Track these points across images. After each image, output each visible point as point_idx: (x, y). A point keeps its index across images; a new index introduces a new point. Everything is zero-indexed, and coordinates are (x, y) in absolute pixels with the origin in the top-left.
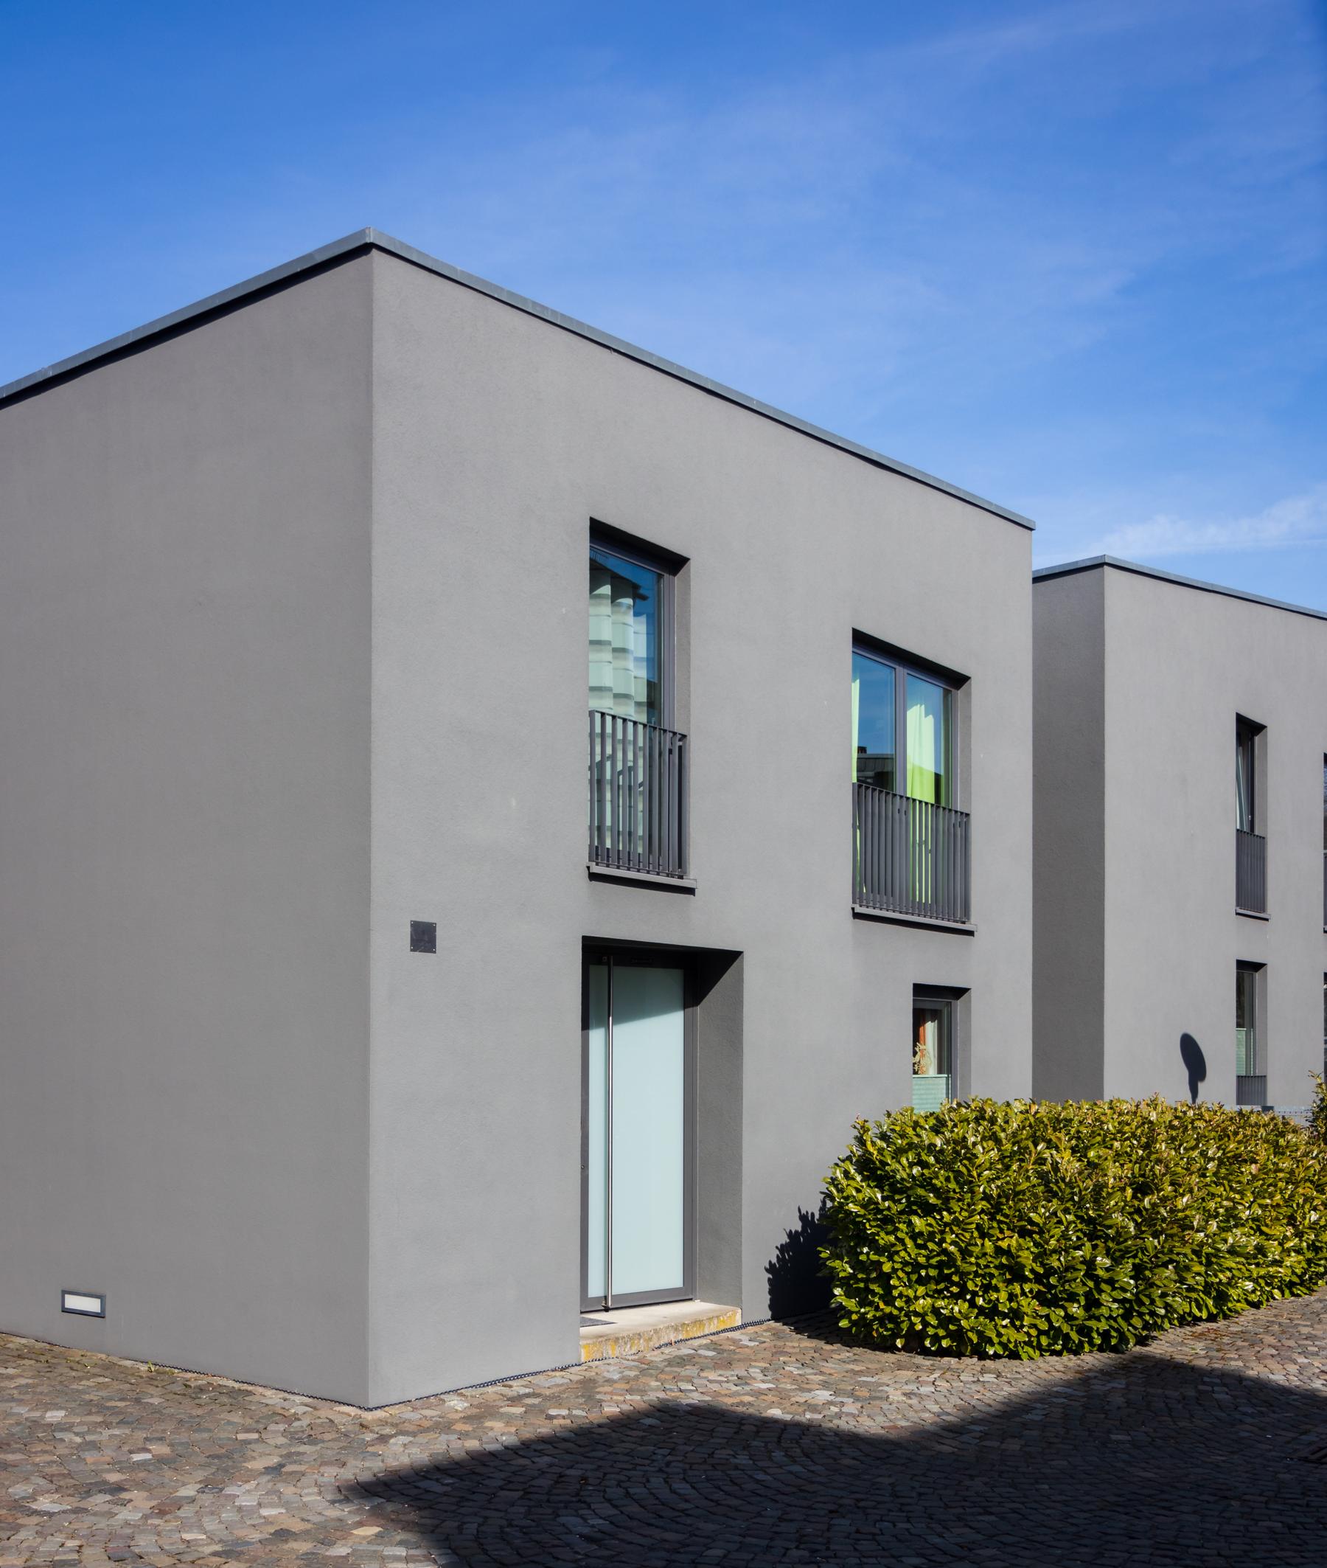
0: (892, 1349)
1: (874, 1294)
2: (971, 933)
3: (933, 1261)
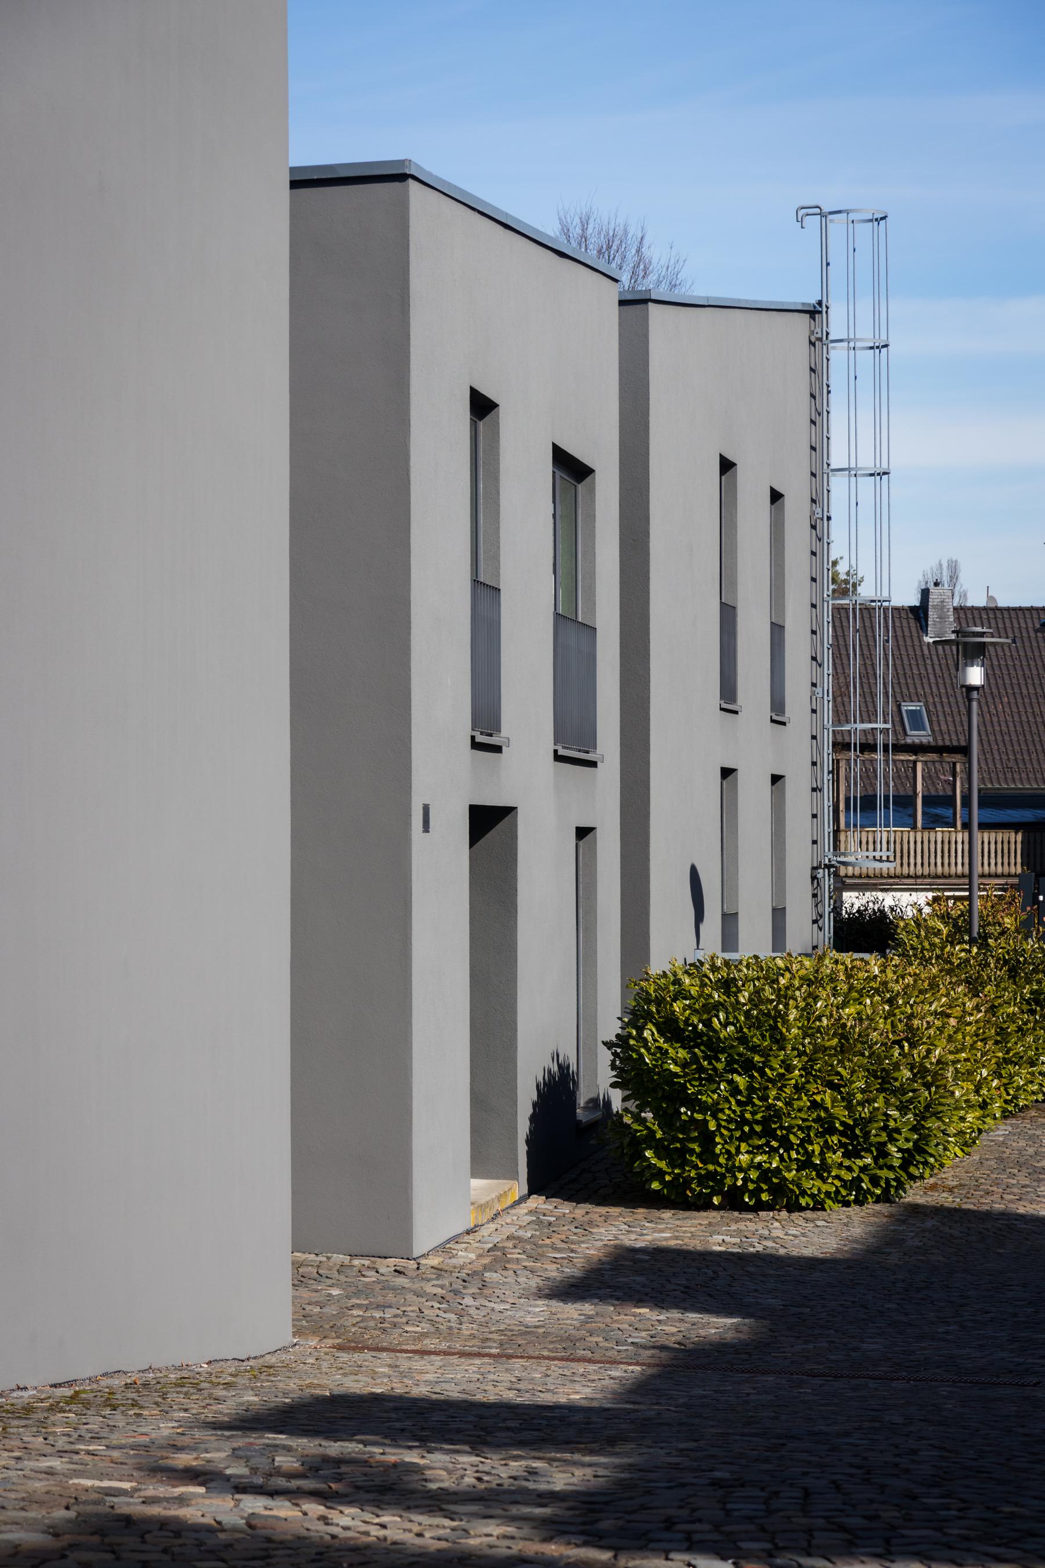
0: (708, 1206)
1: (692, 1151)
2: (593, 764)
3: (758, 1117)
